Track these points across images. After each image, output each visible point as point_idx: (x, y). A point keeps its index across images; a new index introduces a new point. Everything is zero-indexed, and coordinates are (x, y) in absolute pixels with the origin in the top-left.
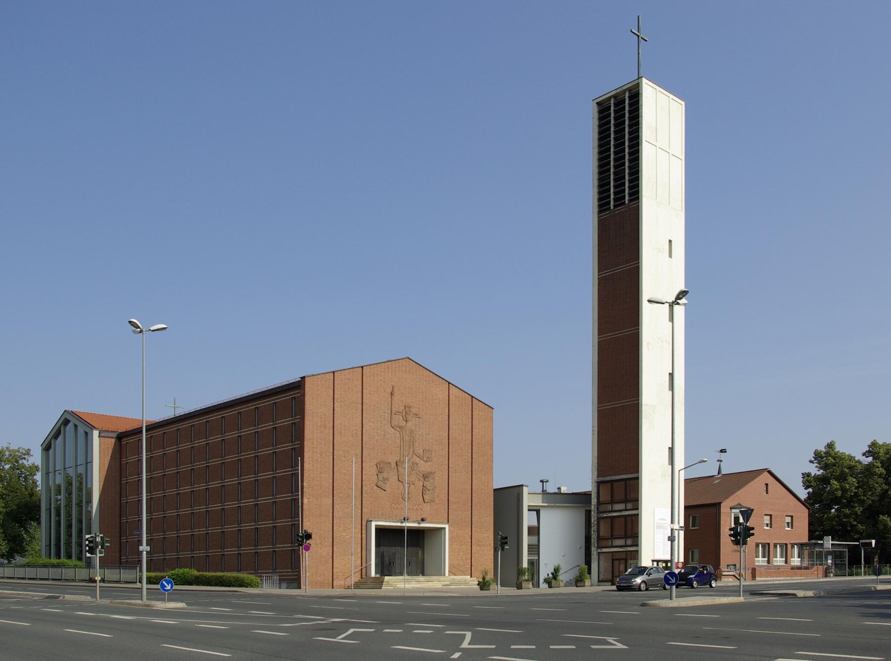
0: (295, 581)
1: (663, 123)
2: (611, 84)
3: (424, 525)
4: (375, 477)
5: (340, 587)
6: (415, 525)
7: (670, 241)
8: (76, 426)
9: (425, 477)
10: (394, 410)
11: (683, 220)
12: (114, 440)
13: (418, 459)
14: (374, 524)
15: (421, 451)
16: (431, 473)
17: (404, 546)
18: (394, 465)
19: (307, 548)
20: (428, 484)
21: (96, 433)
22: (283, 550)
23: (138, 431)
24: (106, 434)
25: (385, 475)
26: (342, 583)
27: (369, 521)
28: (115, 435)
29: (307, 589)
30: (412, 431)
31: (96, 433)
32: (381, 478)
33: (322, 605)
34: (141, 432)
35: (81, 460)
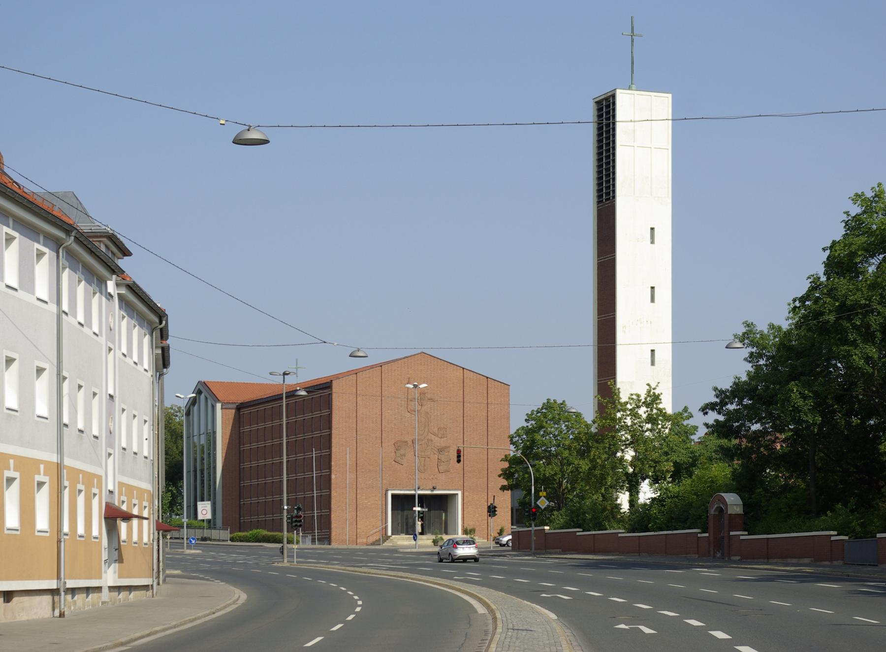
0: (326, 538)
1: (646, 128)
2: (601, 92)
3: (436, 492)
4: (393, 454)
5: (363, 544)
6: (429, 492)
7: (652, 229)
8: (206, 398)
9: (440, 450)
10: (410, 397)
11: (670, 201)
12: (234, 411)
13: (433, 437)
14: (390, 493)
15: (436, 430)
16: (446, 447)
17: (424, 510)
18: (410, 443)
19: (555, 401)
20: (443, 457)
21: (219, 406)
22: (313, 518)
23: (279, 398)
24: (227, 406)
25: (402, 452)
26: (365, 540)
27: (387, 490)
28: (235, 406)
29: (334, 545)
30: (427, 413)
31: (219, 406)
32: (398, 454)
33: (349, 557)
34: (282, 398)
35: (210, 427)
